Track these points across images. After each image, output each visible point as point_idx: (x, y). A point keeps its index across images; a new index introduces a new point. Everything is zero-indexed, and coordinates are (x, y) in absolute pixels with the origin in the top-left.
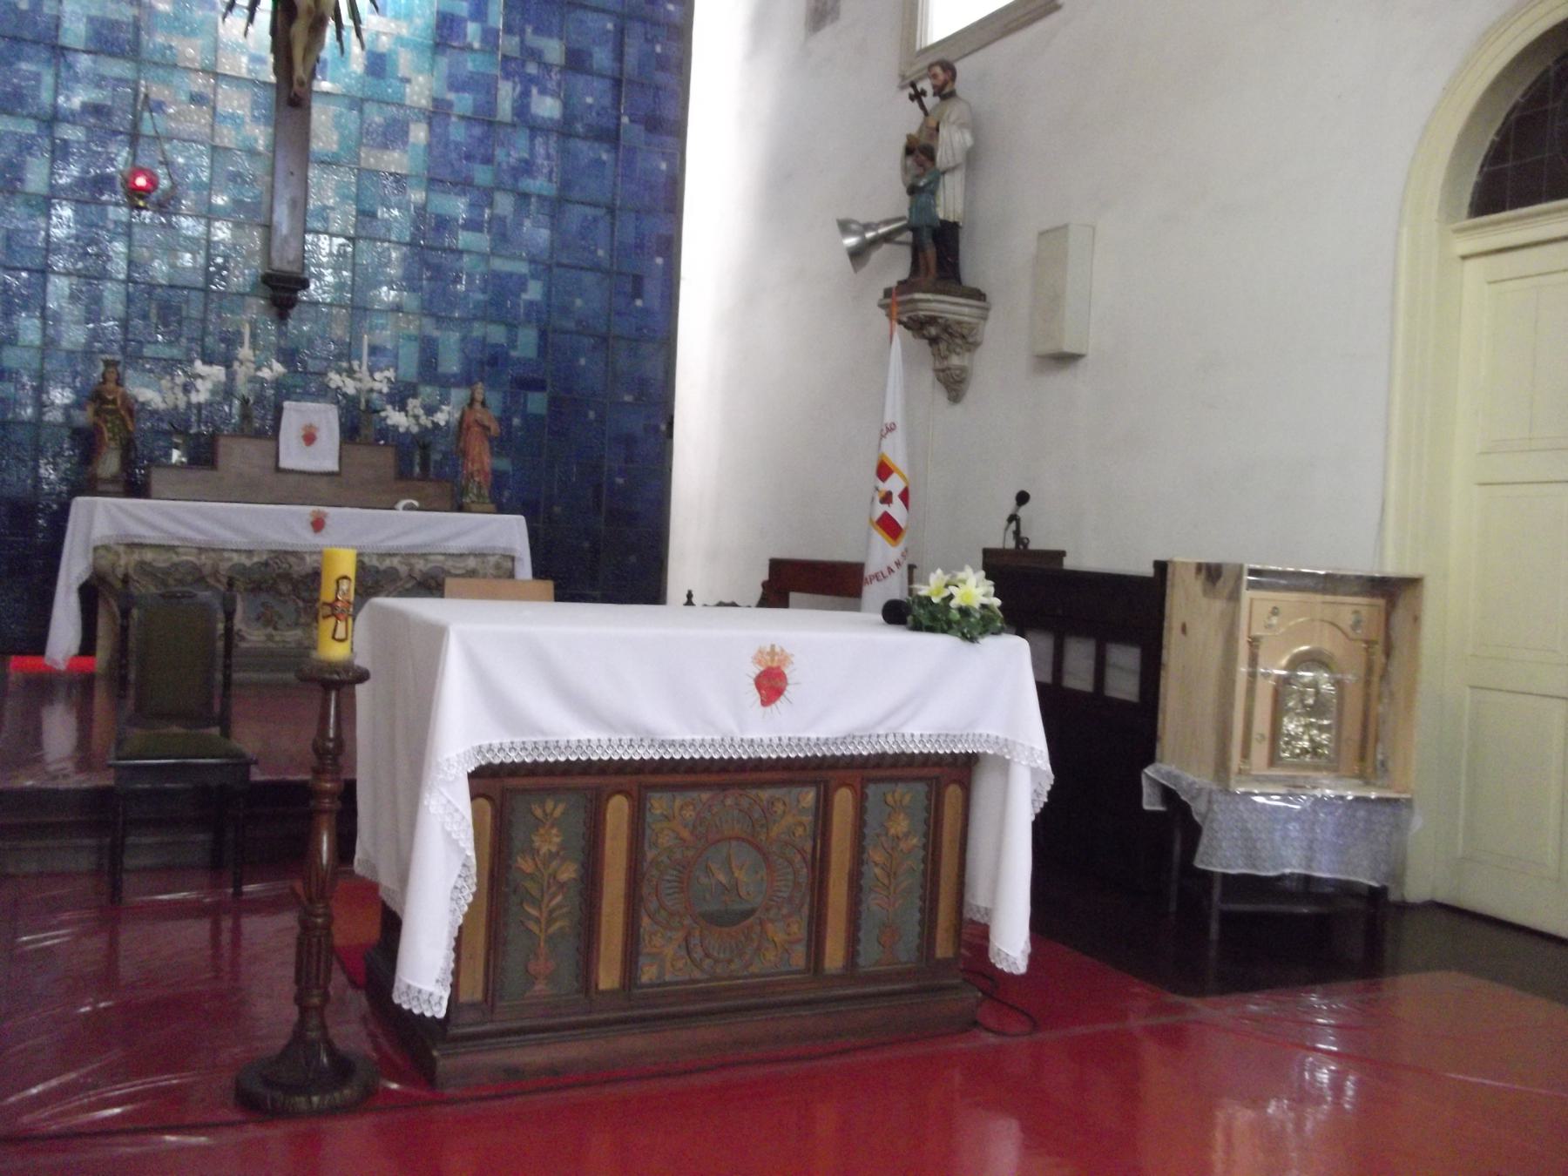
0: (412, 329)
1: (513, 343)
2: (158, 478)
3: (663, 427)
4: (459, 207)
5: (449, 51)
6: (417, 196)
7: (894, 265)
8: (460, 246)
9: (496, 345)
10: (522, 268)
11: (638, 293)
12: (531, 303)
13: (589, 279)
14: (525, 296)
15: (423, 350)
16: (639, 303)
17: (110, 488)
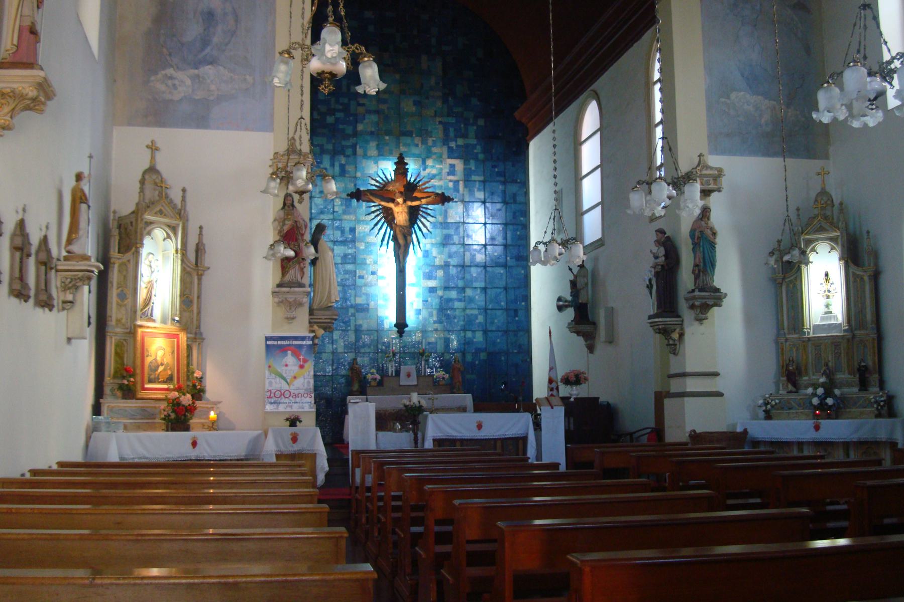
0: (442, 335)
1: (474, 337)
2: (369, 390)
3: (528, 360)
4: (453, 294)
5: (448, 246)
6: (440, 293)
7: (570, 313)
8: (455, 307)
9: (469, 338)
10: (476, 312)
11: (516, 315)
12: (480, 323)
13: (499, 313)
14: (477, 321)
15: (445, 342)
16: (517, 319)
17: (356, 393)
